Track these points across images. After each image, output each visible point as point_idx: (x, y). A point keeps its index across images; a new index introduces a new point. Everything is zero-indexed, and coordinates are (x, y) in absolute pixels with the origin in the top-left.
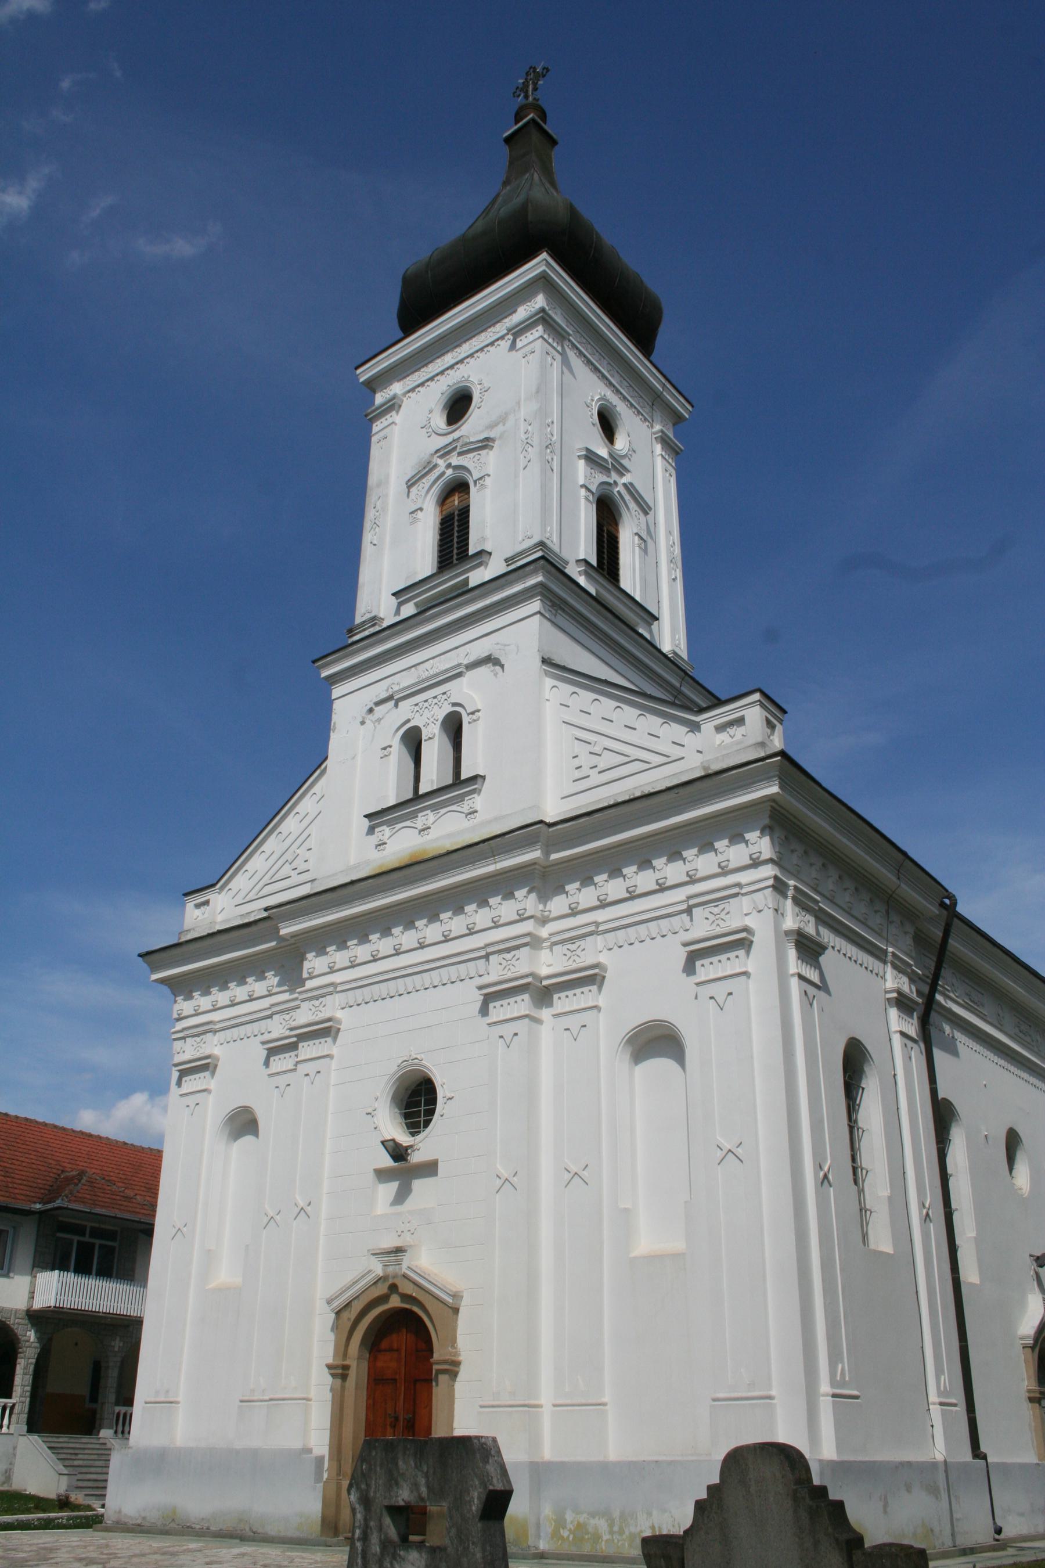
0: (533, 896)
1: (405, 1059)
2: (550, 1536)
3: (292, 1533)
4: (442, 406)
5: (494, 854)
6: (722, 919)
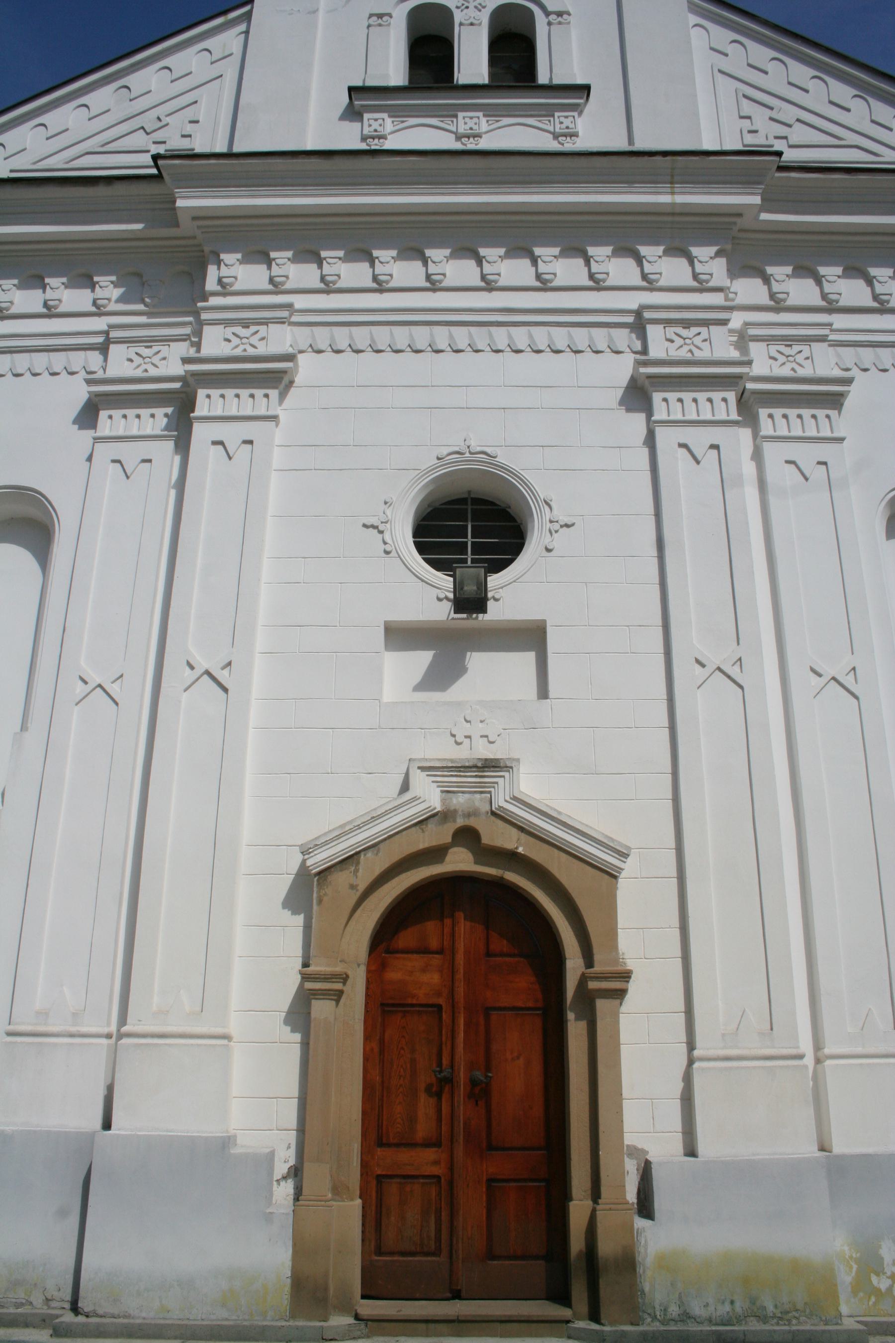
1: (457, 449)
2: (850, 1289)
5: (673, 180)
6: (153, 364)
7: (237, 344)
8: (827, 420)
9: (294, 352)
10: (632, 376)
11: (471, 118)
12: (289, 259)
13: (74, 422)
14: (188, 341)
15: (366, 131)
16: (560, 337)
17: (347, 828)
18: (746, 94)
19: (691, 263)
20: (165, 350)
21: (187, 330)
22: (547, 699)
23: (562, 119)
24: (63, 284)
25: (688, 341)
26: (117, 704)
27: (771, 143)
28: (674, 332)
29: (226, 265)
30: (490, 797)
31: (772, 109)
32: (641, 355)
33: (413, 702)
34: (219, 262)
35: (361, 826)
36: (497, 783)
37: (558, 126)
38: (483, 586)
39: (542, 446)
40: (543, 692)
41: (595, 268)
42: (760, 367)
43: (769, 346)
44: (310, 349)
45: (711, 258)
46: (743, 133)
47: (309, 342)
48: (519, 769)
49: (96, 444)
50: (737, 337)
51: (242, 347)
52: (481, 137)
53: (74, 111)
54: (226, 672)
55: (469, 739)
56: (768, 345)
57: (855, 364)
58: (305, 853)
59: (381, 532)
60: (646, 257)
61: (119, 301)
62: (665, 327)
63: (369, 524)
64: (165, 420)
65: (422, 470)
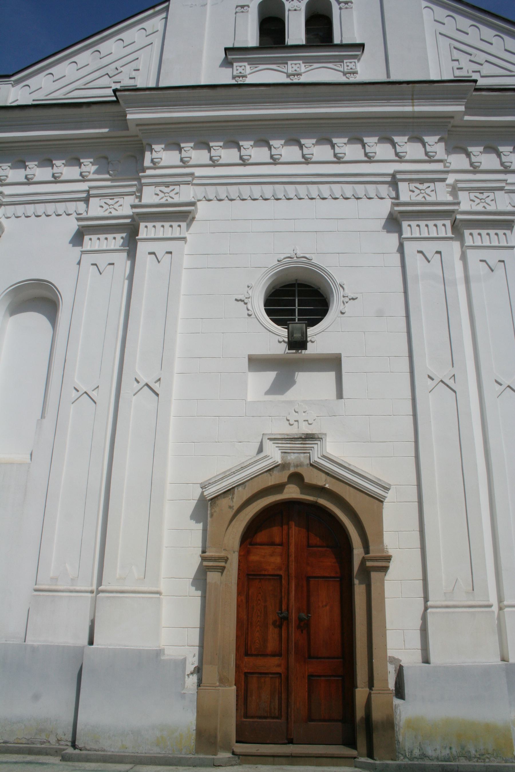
0: (442, 145)
1: (289, 255)
3: (155, 751)
5: (413, 98)
6: (114, 209)
9: (195, 200)
10: (390, 212)
11: (296, 64)
12: (192, 148)
14: (134, 195)
15: (235, 73)
16: (348, 190)
17: (227, 474)
18: (455, 46)
19: (424, 146)
20: (121, 201)
21: (134, 189)
23: (348, 64)
24: (63, 164)
25: (422, 191)
26: (95, 403)
27: (470, 75)
28: (415, 187)
31: (471, 55)
32: (395, 200)
33: (264, 401)
34: (151, 150)
35: (235, 472)
36: (313, 447)
37: (346, 68)
38: (305, 335)
40: (340, 395)
41: (368, 150)
42: (464, 207)
43: (470, 193)
44: (204, 199)
45: (436, 143)
46: (454, 69)
48: (326, 440)
49: (82, 255)
50: (451, 189)
51: (165, 198)
52: (301, 75)
54: (157, 384)
56: (469, 193)
58: (203, 488)
59: (246, 304)
61: (95, 173)
62: (409, 183)
63: (239, 299)
64: (122, 241)
65: (269, 268)
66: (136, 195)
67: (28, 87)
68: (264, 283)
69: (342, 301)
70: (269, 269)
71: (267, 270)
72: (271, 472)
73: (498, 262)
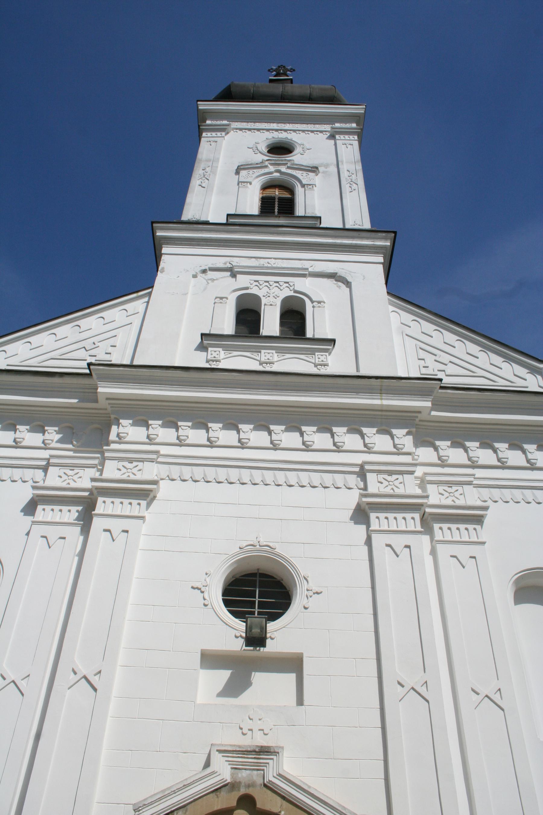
1: (252, 543)
4: (267, 144)
5: (381, 392)
7: (124, 472)
8: (474, 531)
9: (158, 479)
10: (358, 503)
11: (269, 353)
12: (159, 425)
13: (22, 511)
14: (96, 468)
15: (209, 357)
16: (316, 478)
17: (166, 793)
18: (421, 347)
19: (393, 438)
20: (81, 472)
21: (96, 462)
22: (302, 706)
23: (320, 356)
24: (27, 429)
25: (391, 483)
26: (23, 695)
28: (383, 478)
29: (123, 426)
30: (263, 773)
31: (436, 355)
32: (363, 491)
33: (216, 704)
34: (118, 424)
35: (176, 791)
36: (268, 763)
37: (317, 360)
38: (264, 630)
39: (303, 543)
40: (300, 701)
41: (337, 439)
42: (434, 499)
43: (439, 487)
44: (167, 478)
45: (404, 436)
46: (420, 368)
47: (167, 473)
48: (283, 754)
49: (33, 525)
50: (420, 481)
51: (127, 474)
52: (274, 364)
53: (48, 336)
54: (97, 677)
55: (251, 732)
56: (438, 486)
57: (490, 498)
58: (136, 810)
59: (202, 592)
60: (367, 434)
61: (58, 442)
62: (377, 475)
63: (195, 586)
64: (77, 514)
65: (230, 555)
66: (97, 468)
67: (4, 352)
68: (225, 569)
69: (305, 595)
70: (229, 556)
71: (228, 557)
72: (218, 793)
73: (470, 559)
